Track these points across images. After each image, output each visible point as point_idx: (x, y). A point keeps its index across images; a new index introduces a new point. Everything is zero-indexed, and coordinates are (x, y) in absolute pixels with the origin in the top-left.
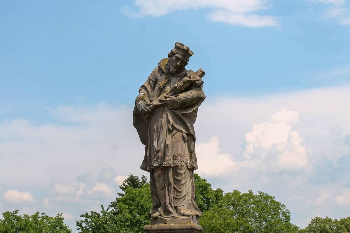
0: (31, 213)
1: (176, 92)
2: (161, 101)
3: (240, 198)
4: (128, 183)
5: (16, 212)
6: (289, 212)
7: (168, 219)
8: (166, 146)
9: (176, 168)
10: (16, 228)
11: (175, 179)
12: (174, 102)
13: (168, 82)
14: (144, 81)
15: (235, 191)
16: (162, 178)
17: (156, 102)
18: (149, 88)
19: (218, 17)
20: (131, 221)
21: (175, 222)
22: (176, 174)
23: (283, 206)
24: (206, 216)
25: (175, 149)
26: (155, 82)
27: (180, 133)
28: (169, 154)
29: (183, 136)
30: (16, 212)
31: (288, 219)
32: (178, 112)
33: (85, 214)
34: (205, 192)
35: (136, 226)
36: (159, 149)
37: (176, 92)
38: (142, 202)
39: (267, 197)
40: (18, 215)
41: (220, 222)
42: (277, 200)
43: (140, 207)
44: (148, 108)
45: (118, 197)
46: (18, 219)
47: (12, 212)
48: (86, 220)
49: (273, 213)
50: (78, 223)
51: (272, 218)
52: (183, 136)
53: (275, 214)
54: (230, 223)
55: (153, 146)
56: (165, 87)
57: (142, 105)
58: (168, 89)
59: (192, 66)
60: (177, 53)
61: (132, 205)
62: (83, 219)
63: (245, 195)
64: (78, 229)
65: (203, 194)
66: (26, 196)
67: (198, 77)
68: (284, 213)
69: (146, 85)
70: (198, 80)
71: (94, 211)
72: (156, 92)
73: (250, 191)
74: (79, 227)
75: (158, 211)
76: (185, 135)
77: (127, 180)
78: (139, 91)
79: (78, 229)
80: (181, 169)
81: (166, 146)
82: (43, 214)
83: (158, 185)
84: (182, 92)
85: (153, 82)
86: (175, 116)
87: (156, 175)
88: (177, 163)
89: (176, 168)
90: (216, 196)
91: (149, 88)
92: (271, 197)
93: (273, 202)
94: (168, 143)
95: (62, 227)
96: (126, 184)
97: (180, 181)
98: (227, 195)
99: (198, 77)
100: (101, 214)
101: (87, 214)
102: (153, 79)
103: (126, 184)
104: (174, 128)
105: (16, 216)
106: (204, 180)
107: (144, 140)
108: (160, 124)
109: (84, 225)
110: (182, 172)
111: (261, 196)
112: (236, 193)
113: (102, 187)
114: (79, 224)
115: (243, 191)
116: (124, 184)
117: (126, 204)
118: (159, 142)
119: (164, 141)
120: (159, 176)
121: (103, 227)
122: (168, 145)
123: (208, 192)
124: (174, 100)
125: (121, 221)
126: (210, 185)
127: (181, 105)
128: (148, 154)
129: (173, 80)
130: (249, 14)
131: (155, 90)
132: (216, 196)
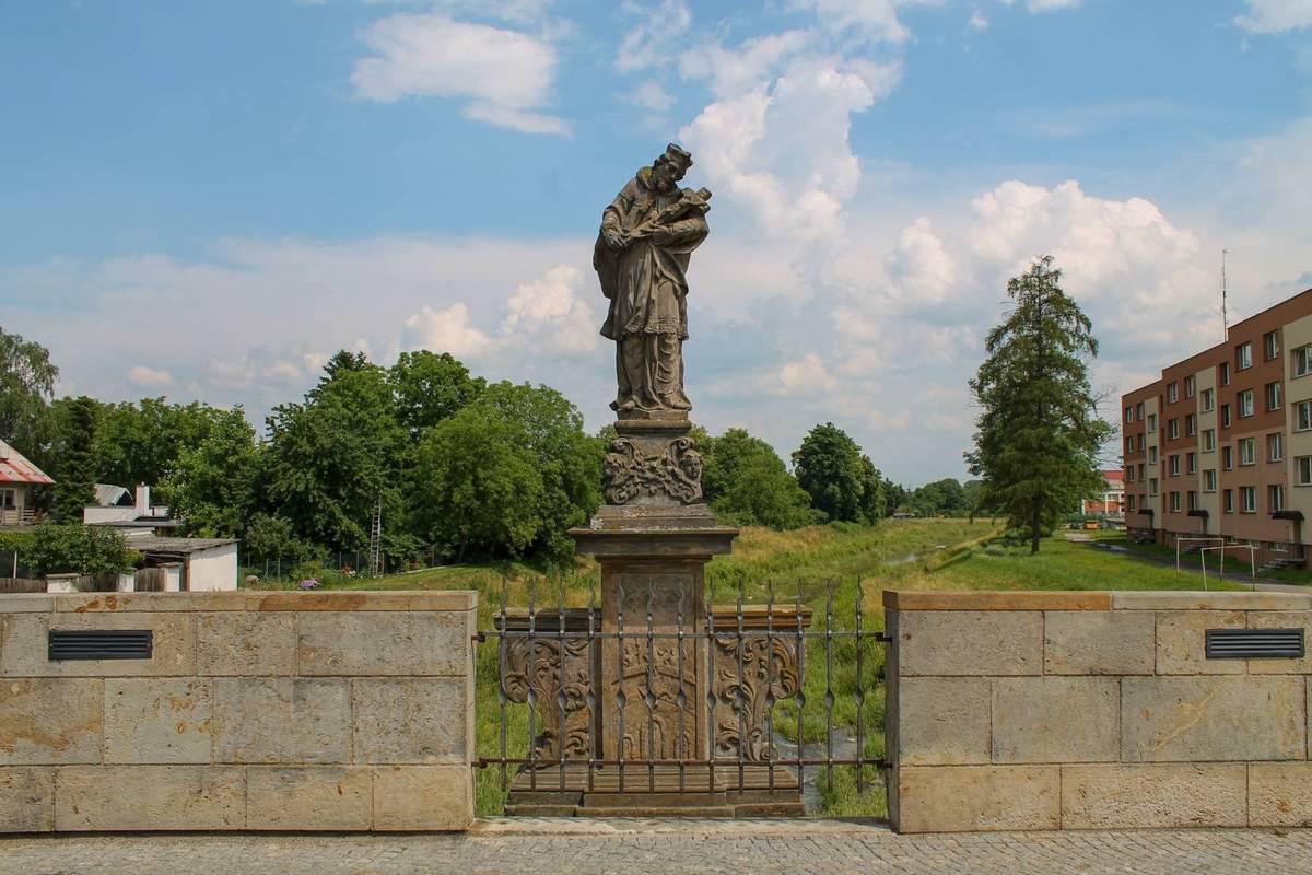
0: (185, 402)
1: (668, 219)
2: (643, 232)
3: (512, 392)
4: (337, 363)
5: (162, 399)
6: (581, 415)
7: (652, 411)
8: (650, 301)
9: (663, 337)
10: (162, 425)
11: (660, 352)
12: (665, 235)
13: (654, 205)
14: (611, 198)
15: (504, 381)
16: (638, 350)
17: (636, 233)
18: (621, 211)
19: (476, 113)
20: (350, 419)
21: (662, 416)
22: (663, 345)
23: (573, 406)
24: (463, 417)
25: (663, 307)
26: (631, 203)
27: (669, 283)
28: (655, 314)
29: (675, 289)
30: (162, 399)
31: (579, 426)
32: (668, 251)
33: (278, 407)
34: (459, 381)
35: (357, 427)
36: (638, 305)
37: (668, 219)
38: (363, 392)
39: (552, 392)
40: (165, 404)
41: (482, 426)
42: (564, 397)
43: (359, 400)
44: (624, 241)
45: (321, 383)
46: (165, 410)
47: (155, 399)
48: (281, 416)
49: (558, 416)
50: (267, 419)
51: (557, 423)
52: (675, 289)
53: (562, 418)
54: (497, 428)
55: (627, 300)
56: (648, 210)
57: (615, 236)
58: (654, 214)
59: (689, 182)
60: (673, 160)
61: (347, 395)
62: (277, 414)
63: (520, 388)
64: (268, 429)
65: (456, 384)
66: (163, 377)
67: (702, 201)
68: (574, 417)
69: (617, 206)
70: (703, 205)
71: (293, 402)
72: (634, 218)
73: (527, 382)
74: (269, 426)
75: (632, 399)
76: (678, 287)
77: (336, 358)
78: (605, 214)
79: (268, 429)
80: (670, 338)
81: (650, 301)
82: (205, 404)
83: (628, 360)
84: (675, 220)
85: (628, 201)
86: (664, 256)
87: (628, 345)
88: (667, 329)
89: (663, 337)
90: (476, 387)
91: (621, 211)
92: (556, 393)
93: (558, 399)
94: (654, 297)
95: (241, 426)
96: (334, 364)
97: (669, 355)
98: (493, 387)
99: (702, 201)
100: (305, 408)
101: (282, 406)
102: (628, 196)
103: (334, 364)
104: (662, 274)
105: (162, 406)
106: (459, 364)
107: (608, 291)
108: (640, 266)
109: (277, 423)
110: (672, 342)
111: (542, 390)
112: (506, 384)
113: (289, 369)
114: (269, 421)
115: (516, 382)
116: (331, 364)
117: (338, 394)
118: (639, 296)
119: (647, 293)
120: (635, 347)
121: (310, 428)
122: (653, 301)
123: (464, 382)
124: (665, 232)
125: (335, 420)
126: (467, 371)
127: (675, 241)
128: (616, 312)
129: (662, 201)
130: (522, 111)
131: (630, 214)
132: (476, 387)
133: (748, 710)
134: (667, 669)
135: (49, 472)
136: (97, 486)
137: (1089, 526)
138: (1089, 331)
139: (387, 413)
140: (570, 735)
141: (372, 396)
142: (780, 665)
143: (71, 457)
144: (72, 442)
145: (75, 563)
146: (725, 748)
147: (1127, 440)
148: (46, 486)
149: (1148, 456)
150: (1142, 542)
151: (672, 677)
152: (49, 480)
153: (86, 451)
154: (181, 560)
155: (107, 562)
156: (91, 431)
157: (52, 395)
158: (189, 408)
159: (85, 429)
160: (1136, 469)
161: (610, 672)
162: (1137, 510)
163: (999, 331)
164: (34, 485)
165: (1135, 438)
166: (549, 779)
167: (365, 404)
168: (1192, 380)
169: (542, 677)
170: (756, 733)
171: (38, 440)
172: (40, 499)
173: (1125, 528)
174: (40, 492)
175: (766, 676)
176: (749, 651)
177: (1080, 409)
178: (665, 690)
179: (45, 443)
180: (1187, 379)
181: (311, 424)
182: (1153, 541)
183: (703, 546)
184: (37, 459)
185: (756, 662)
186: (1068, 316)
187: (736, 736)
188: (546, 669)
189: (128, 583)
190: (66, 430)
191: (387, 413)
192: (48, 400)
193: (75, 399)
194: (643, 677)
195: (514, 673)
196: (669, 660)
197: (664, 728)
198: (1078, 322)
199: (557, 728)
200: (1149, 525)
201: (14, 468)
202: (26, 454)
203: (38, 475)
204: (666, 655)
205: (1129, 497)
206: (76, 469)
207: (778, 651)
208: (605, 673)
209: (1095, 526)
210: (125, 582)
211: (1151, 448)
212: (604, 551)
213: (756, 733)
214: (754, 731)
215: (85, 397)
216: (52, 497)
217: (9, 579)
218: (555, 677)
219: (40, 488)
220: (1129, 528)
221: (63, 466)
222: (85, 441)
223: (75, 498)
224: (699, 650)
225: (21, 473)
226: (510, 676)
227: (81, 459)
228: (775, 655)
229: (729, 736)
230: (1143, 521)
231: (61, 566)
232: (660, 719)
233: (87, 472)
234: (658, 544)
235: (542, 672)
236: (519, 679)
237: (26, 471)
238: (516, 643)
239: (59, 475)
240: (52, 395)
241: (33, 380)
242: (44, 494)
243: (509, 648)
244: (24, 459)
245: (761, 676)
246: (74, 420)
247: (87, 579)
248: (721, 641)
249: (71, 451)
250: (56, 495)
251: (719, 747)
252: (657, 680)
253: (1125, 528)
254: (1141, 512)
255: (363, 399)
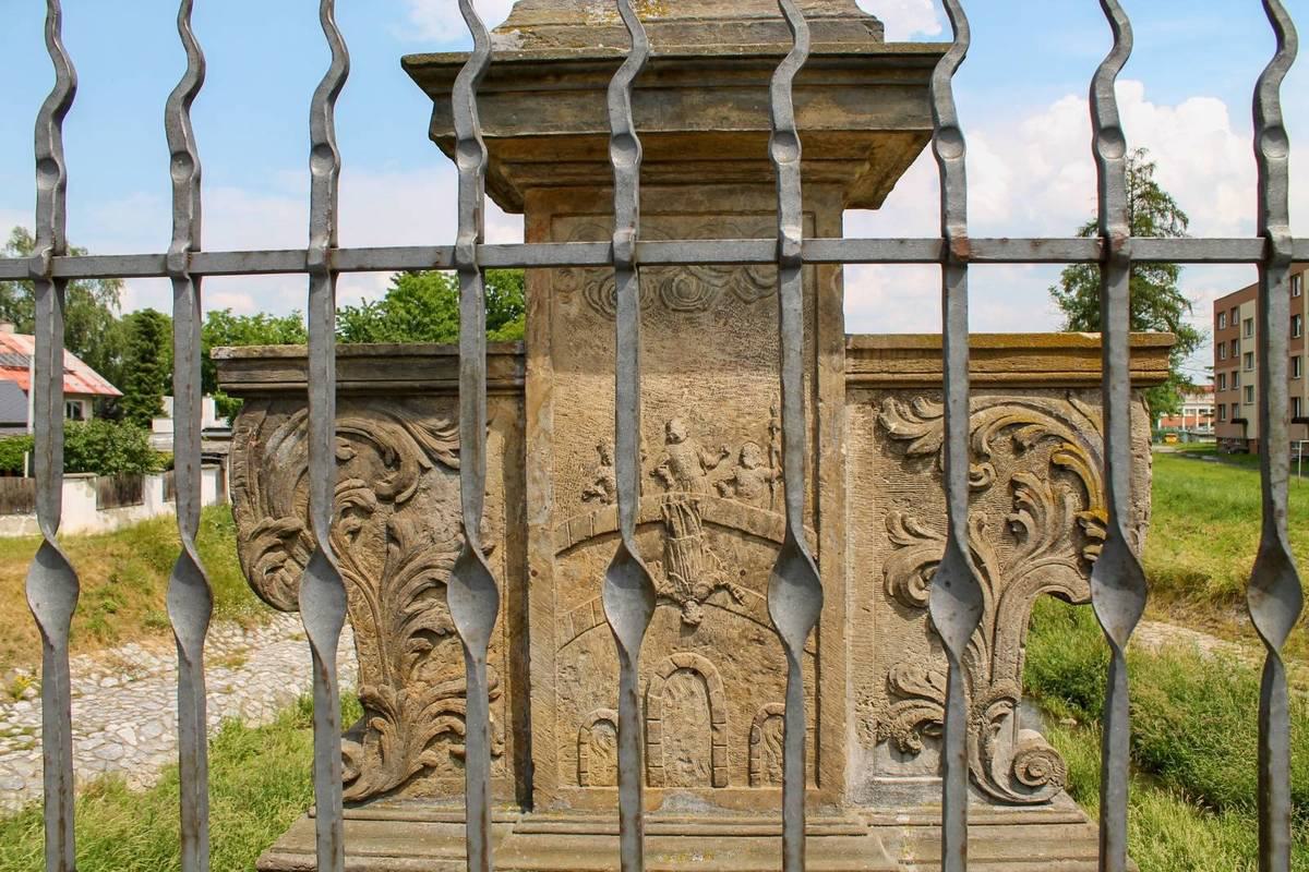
0: (251, 314)
5: (228, 311)
38: (426, 297)
40: (231, 315)
46: (231, 322)
47: (221, 311)
61: (409, 302)
71: (349, 305)
82: (270, 315)
100: (361, 311)
121: (365, 330)
133: (980, 644)
134: (728, 511)
135: (118, 386)
136: (164, 398)
137: (1168, 439)
138: (1185, 227)
139: (451, 318)
140: (436, 707)
141: (434, 302)
142: (1072, 500)
143: (138, 369)
144: (139, 354)
145: (93, 461)
146: (904, 752)
147: (1218, 346)
148: (117, 398)
149: (1242, 362)
150: (1235, 452)
151: (745, 534)
152: (117, 392)
153: (153, 362)
154: (218, 462)
155: (127, 461)
156: (157, 343)
157: (119, 307)
158: (256, 319)
159: (150, 341)
160: (1229, 378)
161: (551, 518)
162: (1228, 419)
163: (1088, 229)
164: (105, 397)
165: (1228, 344)
166: (376, 838)
167: (426, 309)
168: (1299, 279)
169: (355, 533)
170: (998, 709)
171: (107, 355)
172: (110, 412)
173: (1215, 441)
174: (112, 405)
175: (1032, 531)
176: (979, 456)
177: (1174, 309)
178: (722, 576)
179: (115, 356)
180: (1234, 309)
181: (366, 327)
182: (1246, 452)
183: (840, 104)
184: (107, 373)
185: (999, 491)
186: (1162, 212)
187: (937, 713)
188: (366, 512)
189: (155, 485)
190: (133, 342)
191: (451, 318)
192: (117, 315)
193: (142, 311)
194: (656, 533)
195: (271, 522)
196: (734, 482)
197: (718, 690)
198: (1174, 219)
199: (399, 685)
200: (1242, 435)
201: (82, 380)
202: (95, 368)
203: (106, 387)
204: (725, 469)
205: (1220, 407)
206: (143, 381)
207: (1066, 459)
208: (536, 521)
209: (1175, 439)
210: (152, 485)
211: (1246, 354)
212: (521, 124)
213: (998, 709)
214: (994, 701)
215: (150, 309)
216: (122, 409)
217: (20, 479)
218: (392, 536)
219: (111, 401)
220: (1219, 439)
221: (130, 378)
222: (152, 353)
223: (143, 410)
224: (827, 452)
225: (88, 385)
226: (265, 530)
227: (148, 371)
228: (1058, 470)
229: (917, 715)
230: (1237, 431)
231: (76, 465)
232: (705, 664)
233: (154, 383)
234: (696, 98)
235: (354, 521)
236: (289, 537)
237: (92, 383)
238: (279, 433)
239: (127, 387)
240: (119, 307)
241: (100, 294)
242: (115, 407)
243: (260, 447)
244: (93, 372)
245: (1015, 532)
246: (140, 332)
247: (106, 479)
248: (893, 426)
249: (139, 363)
250: (126, 407)
251: (885, 747)
252: (694, 545)
253: (1215, 441)
254: (1234, 421)
255: (425, 304)
